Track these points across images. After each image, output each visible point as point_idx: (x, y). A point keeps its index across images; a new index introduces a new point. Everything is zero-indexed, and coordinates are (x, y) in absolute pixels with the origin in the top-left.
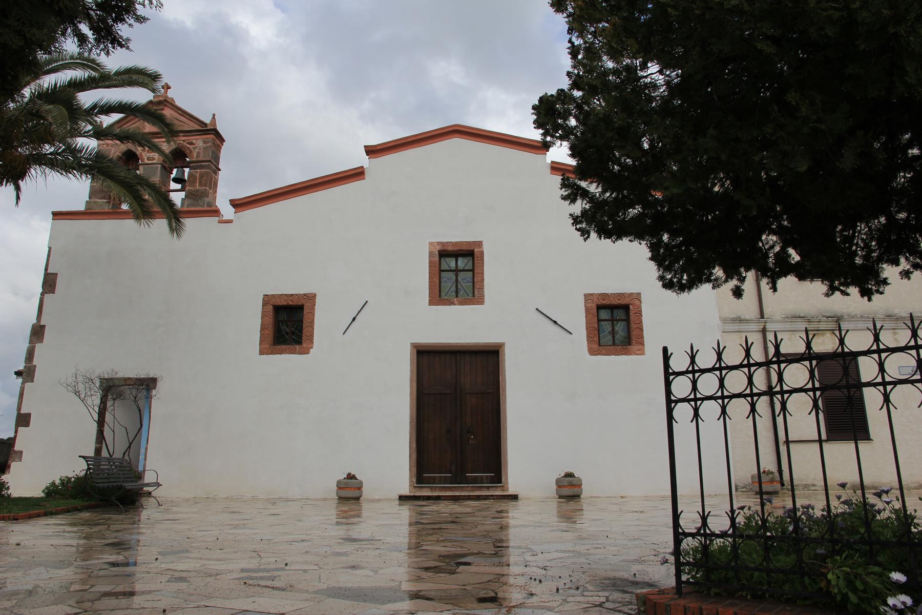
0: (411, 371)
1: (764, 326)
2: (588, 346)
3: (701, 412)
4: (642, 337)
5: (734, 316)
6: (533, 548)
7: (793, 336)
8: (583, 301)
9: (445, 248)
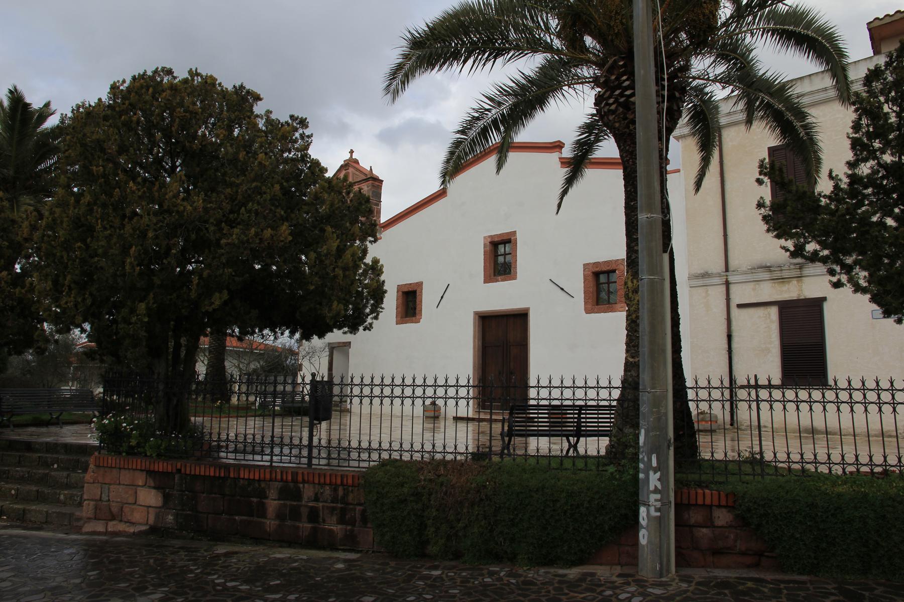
0: (474, 331)
1: (727, 279)
3: (393, 402)
5: (702, 271)
7: (757, 286)
9: (493, 240)
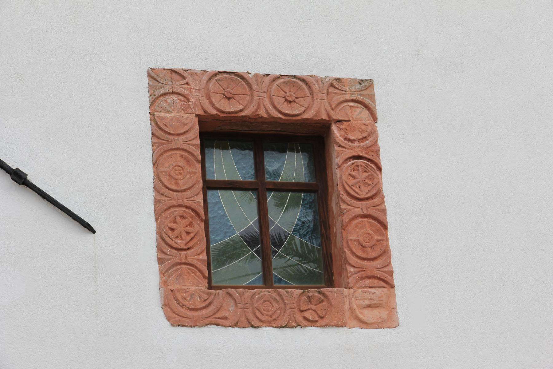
2: (164, 283)
4: (386, 252)
6: (187, 313)
8: (145, 99)
